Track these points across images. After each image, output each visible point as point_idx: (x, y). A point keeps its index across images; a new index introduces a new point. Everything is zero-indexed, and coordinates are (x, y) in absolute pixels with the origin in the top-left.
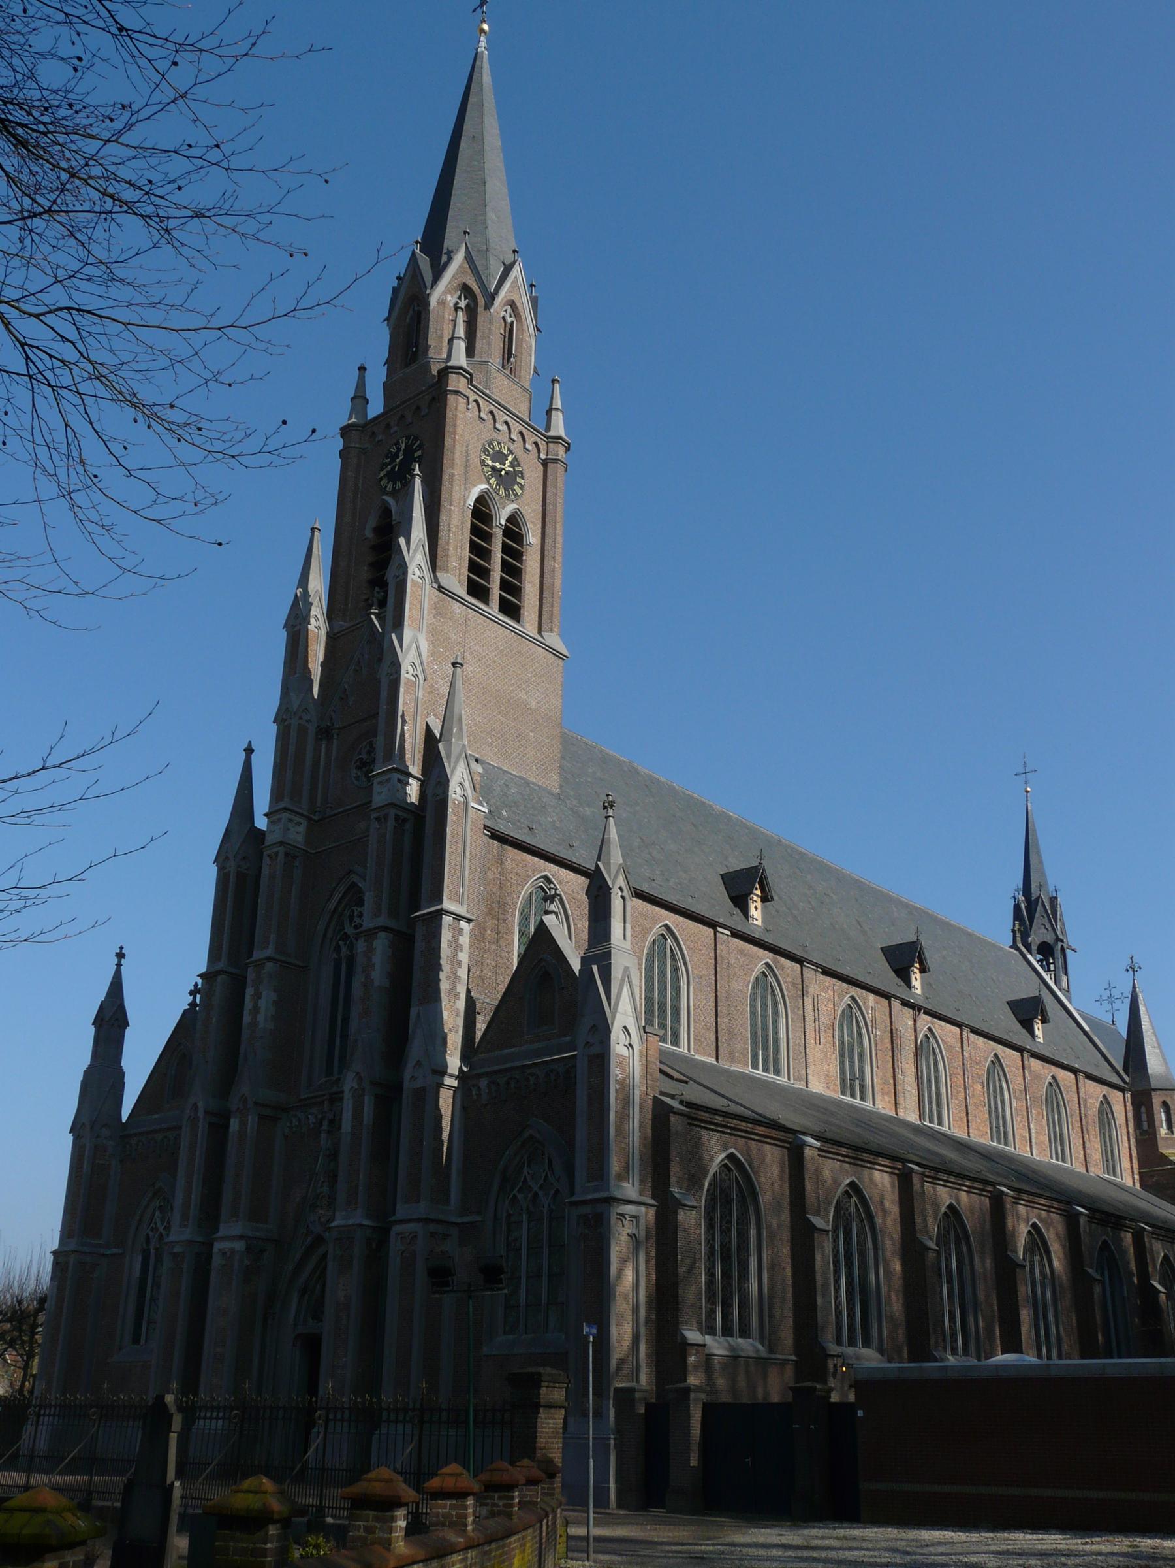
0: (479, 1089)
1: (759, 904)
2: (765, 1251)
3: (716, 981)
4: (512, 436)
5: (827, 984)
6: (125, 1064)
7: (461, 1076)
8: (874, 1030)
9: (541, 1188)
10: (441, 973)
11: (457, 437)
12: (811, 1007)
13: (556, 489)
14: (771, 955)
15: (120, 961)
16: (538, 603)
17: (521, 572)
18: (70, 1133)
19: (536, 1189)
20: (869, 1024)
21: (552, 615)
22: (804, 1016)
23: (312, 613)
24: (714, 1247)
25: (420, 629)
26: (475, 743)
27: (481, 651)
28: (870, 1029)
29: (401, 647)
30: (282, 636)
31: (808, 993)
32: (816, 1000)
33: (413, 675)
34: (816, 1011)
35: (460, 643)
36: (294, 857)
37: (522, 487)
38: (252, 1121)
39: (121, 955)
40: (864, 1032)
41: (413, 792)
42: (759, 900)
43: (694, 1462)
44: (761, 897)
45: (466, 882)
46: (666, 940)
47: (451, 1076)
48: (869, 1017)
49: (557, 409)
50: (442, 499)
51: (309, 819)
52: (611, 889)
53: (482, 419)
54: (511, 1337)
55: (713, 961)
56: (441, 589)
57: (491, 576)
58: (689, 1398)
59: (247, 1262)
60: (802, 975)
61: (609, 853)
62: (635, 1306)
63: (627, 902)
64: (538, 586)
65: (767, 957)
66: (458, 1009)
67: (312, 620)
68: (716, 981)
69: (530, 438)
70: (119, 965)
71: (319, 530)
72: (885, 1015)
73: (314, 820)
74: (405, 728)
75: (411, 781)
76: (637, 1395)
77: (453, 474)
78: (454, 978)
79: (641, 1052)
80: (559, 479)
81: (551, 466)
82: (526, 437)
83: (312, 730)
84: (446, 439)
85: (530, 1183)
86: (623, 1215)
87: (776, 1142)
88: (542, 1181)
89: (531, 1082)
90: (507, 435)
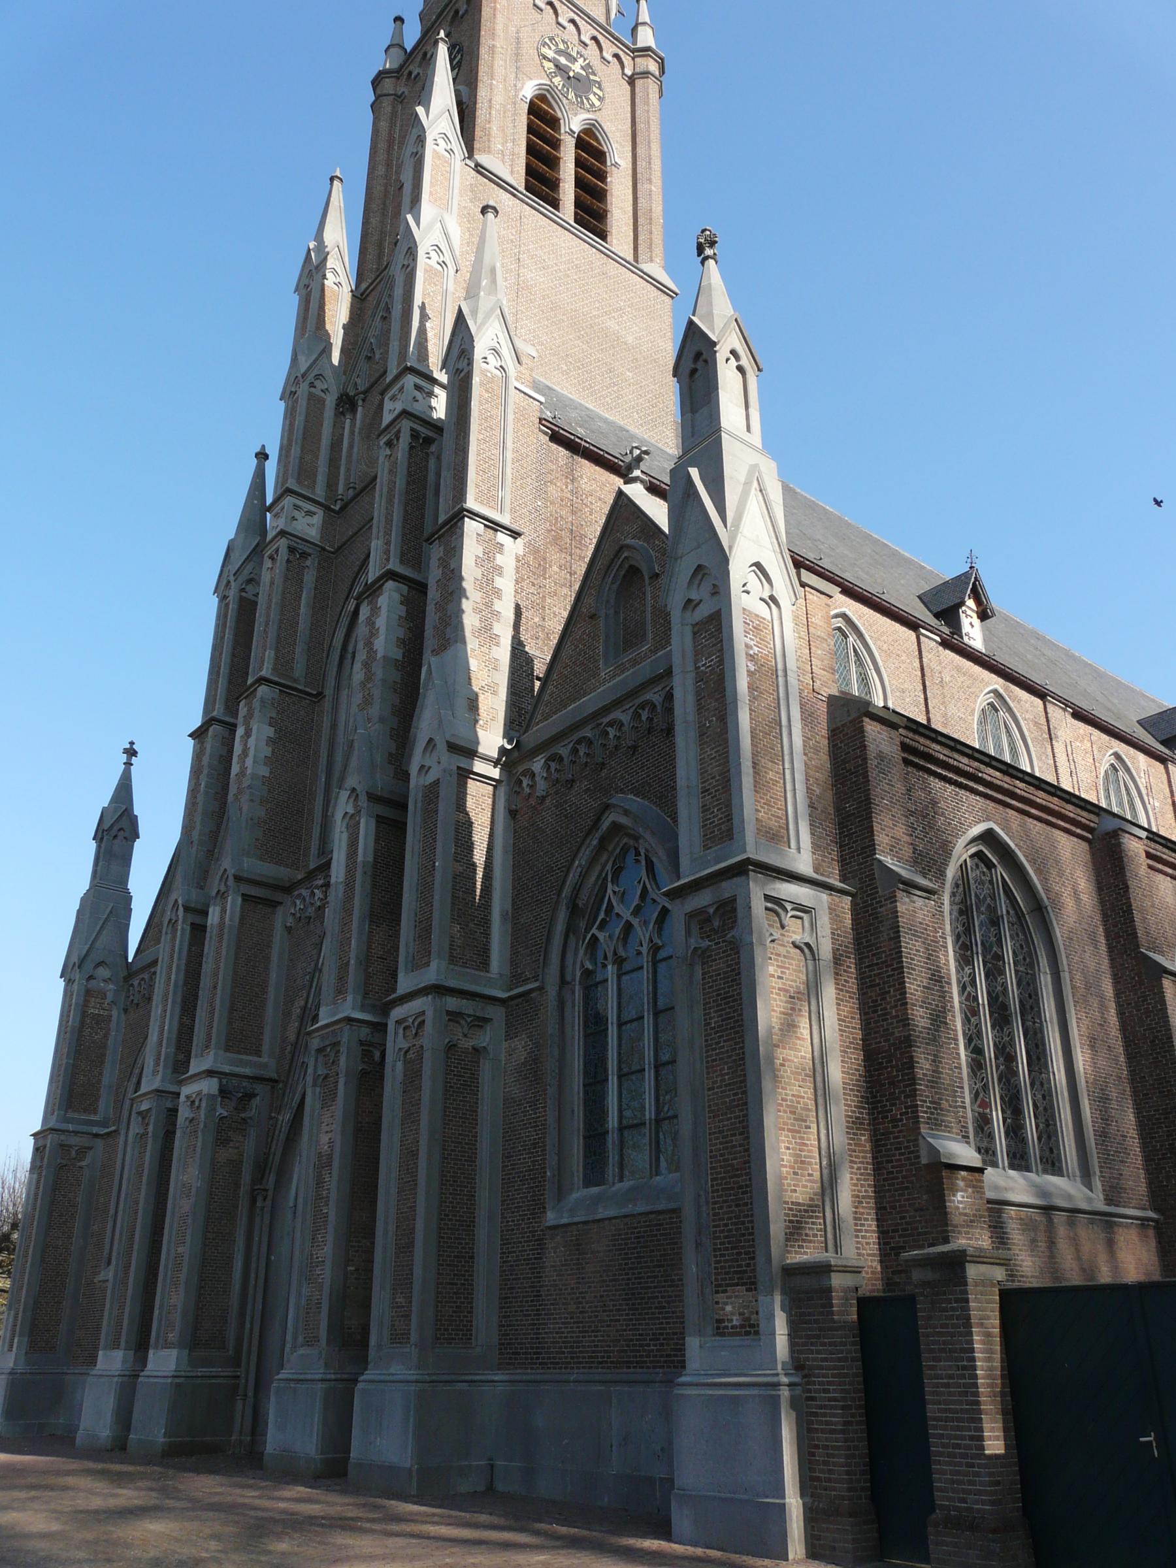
0: (533, 775)
1: (976, 621)
2: (1073, 1012)
3: (926, 699)
4: (583, 38)
5: (1081, 731)
6: (132, 886)
7: (506, 760)
8: (1151, 800)
9: (637, 911)
10: (464, 600)
11: (498, 6)
12: (1064, 755)
13: (648, 105)
14: (1001, 681)
15: (129, 759)
16: (632, 234)
17: (606, 196)
18: (61, 977)
19: (627, 914)
20: (1144, 792)
21: (651, 245)
22: (1056, 766)
23: (330, 264)
24: (976, 998)
25: (447, 207)
26: (541, 365)
27: (546, 257)
28: (1146, 798)
29: (418, 224)
30: (293, 302)
31: (1057, 737)
32: (1069, 747)
33: (439, 263)
34: (1072, 763)
35: (512, 241)
36: (304, 555)
37: (600, 99)
38: (234, 902)
39: (131, 752)
40: (1137, 801)
41: (439, 406)
42: (975, 615)
43: (994, 1444)
44: (977, 613)
45: (508, 482)
46: (846, 637)
47: (486, 759)
48: (1142, 783)
49: (644, 23)
50: (480, 74)
51: (327, 508)
52: (714, 344)
53: (538, 8)
54: (595, 1190)
55: (919, 673)
56: (479, 168)
57: (561, 189)
58: (965, 1277)
59: (220, 1111)
60: (1046, 713)
61: (710, 304)
62: (817, 1061)
63: (748, 376)
64: (631, 214)
65: (997, 683)
66: (497, 660)
67: (329, 275)
68: (926, 699)
69: (609, 50)
70: (128, 764)
71: (341, 180)
72: (1162, 783)
73: (333, 511)
74: (428, 325)
75: (437, 390)
76: (837, 1281)
77: (493, 46)
78: (489, 614)
79: (796, 618)
80: (651, 96)
81: (639, 83)
82: (603, 44)
83: (330, 401)
84: (483, 9)
85: (618, 908)
86: (777, 901)
87: (1072, 827)
88: (636, 901)
89: (611, 736)
90: (577, 37)
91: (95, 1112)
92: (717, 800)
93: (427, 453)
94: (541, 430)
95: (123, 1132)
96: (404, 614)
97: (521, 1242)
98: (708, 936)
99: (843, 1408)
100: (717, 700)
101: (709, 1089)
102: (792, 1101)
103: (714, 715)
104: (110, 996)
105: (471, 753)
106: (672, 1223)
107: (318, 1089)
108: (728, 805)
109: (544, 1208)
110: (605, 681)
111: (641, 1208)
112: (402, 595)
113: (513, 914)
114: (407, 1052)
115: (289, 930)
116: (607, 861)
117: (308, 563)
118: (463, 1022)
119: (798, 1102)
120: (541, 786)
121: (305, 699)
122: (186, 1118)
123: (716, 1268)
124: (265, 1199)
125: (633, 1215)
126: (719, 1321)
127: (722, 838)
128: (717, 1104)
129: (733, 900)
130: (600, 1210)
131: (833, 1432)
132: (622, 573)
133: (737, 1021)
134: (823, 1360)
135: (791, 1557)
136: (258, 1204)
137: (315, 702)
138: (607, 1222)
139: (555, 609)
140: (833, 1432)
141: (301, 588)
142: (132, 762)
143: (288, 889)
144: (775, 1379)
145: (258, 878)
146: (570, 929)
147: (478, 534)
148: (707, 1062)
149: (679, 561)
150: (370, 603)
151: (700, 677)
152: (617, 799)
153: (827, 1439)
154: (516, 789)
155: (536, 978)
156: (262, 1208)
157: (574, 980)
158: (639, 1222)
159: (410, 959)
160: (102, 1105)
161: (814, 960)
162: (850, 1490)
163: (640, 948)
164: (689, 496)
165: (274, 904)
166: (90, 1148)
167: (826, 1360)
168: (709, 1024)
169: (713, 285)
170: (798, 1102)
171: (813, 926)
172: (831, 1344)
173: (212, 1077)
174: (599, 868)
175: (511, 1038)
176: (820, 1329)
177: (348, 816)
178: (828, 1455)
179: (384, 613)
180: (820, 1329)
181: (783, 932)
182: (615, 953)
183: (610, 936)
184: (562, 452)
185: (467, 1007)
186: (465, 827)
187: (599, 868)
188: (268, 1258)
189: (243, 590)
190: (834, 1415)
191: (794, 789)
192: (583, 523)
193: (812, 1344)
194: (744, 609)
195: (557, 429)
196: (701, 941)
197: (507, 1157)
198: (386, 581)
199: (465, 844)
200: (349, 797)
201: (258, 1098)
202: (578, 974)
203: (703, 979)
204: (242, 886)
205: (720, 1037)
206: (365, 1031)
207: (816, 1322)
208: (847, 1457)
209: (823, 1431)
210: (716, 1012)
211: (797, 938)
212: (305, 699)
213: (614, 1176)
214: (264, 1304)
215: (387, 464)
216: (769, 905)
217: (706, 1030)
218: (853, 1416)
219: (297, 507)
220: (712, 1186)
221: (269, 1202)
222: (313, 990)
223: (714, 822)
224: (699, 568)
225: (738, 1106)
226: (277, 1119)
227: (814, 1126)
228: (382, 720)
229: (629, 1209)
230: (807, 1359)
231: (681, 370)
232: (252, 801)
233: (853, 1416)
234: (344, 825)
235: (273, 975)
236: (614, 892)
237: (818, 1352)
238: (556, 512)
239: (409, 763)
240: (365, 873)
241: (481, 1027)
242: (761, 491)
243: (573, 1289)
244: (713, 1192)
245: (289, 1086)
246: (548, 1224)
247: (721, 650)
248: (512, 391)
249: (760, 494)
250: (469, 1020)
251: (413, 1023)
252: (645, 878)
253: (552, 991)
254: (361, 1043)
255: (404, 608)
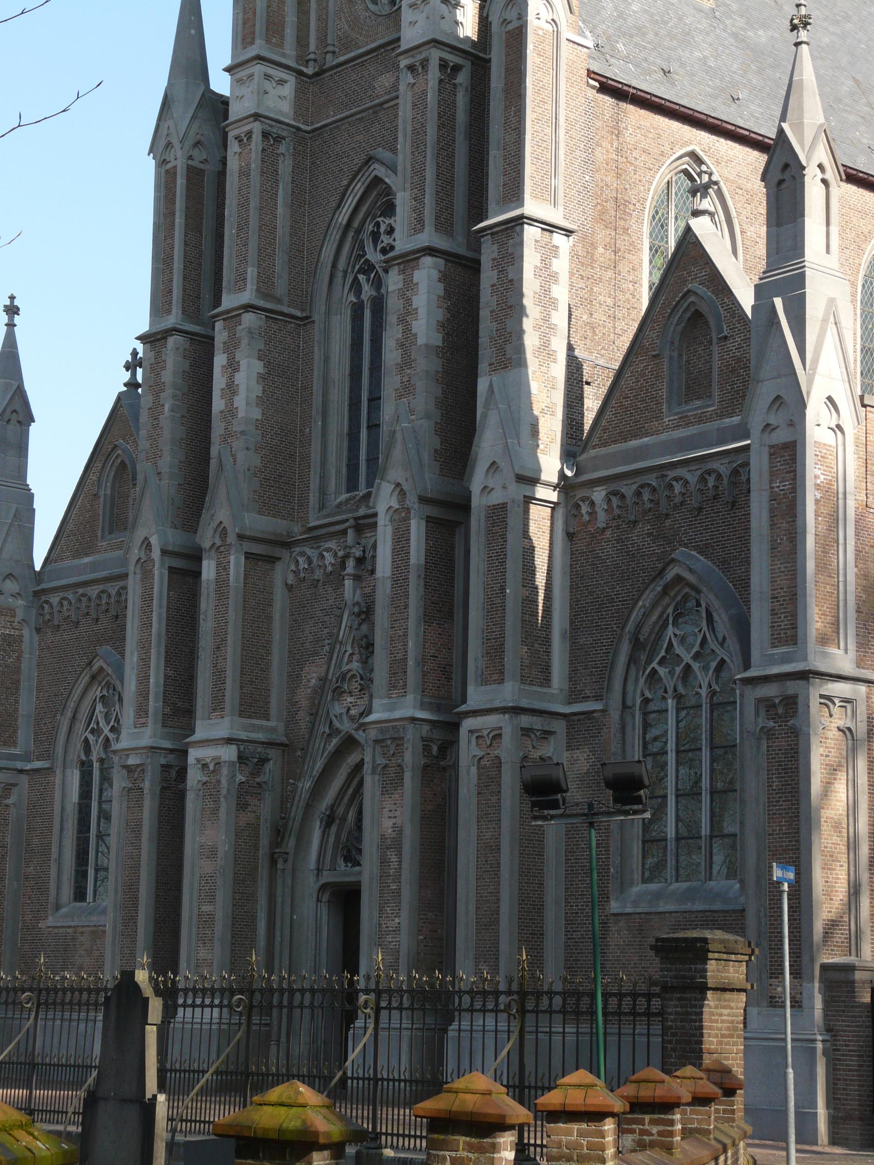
0: (592, 504)
6: (32, 480)
7: (564, 485)
9: (697, 657)
15: (11, 319)
19: (687, 658)
36: (279, 139)
38: (236, 562)
39: (12, 310)
47: (547, 484)
52: (804, 168)
54: (653, 887)
59: (240, 778)
63: (831, 189)
70: (11, 325)
76: (858, 975)
78: (546, 327)
86: (829, 698)
88: (696, 648)
89: (676, 491)
91: (14, 744)
92: (785, 608)
93: (455, 85)
94: (588, 85)
95: (58, 771)
96: (442, 293)
97: (585, 924)
98: (773, 719)
99: (858, 1056)
100: (788, 522)
101: (770, 835)
102: (831, 848)
103: (785, 535)
104: (20, 614)
105: (534, 480)
106: (726, 920)
107: (377, 777)
108: (794, 615)
109: (608, 898)
110: (667, 428)
111: (698, 906)
112: (440, 271)
113: (571, 633)
114: (481, 758)
115: (290, 588)
116: (668, 605)
117: (282, 149)
118: (533, 736)
119: (836, 848)
120: (602, 518)
121: (291, 323)
122: (199, 781)
123: (771, 961)
124: (286, 861)
125: (692, 912)
126: (771, 997)
127: (787, 641)
128: (776, 847)
129: (795, 697)
130: (662, 904)
131: (850, 1070)
132: (688, 315)
133: (794, 788)
134: (846, 1026)
135: (819, 1143)
136: (280, 866)
137: (300, 325)
138: (667, 915)
139: (601, 297)
140: (850, 1070)
141: (277, 182)
142: (16, 322)
143: (287, 544)
144: (813, 1037)
145: (260, 536)
146: (632, 660)
147: (536, 241)
148: (769, 814)
149: (760, 384)
150: (402, 272)
151: (773, 498)
152: (680, 553)
153: (846, 1075)
154: (574, 512)
155: (598, 698)
156: (283, 870)
157: (634, 705)
158: (697, 917)
159: (479, 673)
160: (21, 735)
161: (853, 740)
162: (859, 1105)
163: (699, 690)
164: (772, 325)
165: (272, 560)
166: (15, 785)
167: (849, 1026)
168: (771, 786)
169: (805, 82)
170: (836, 848)
171: (854, 713)
172: (852, 1016)
173: (231, 744)
174: (659, 609)
175: (572, 750)
176: (845, 1007)
177: (391, 511)
178: (847, 1085)
179: (423, 289)
180: (845, 1007)
181: (831, 719)
182: (675, 690)
183: (669, 672)
184: (608, 101)
185: (536, 722)
186: (530, 550)
187: (659, 609)
188: (292, 918)
189: (190, 158)
190: (853, 1061)
191: (846, 600)
192: (628, 186)
193: (839, 1016)
194: (815, 442)
195: (604, 80)
196: (766, 721)
197: (570, 852)
198: (424, 255)
199: (530, 570)
200: (393, 491)
201: (271, 762)
202: (639, 701)
203: (768, 751)
204: (244, 544)
205: (780, 797)
206: (426, 728)
207: (843, 1001)
208: (859, 1086)
209: (844, 1070)
210: (777, 778)
211: (841, 723)
212: (291, 323)
213: (672, 877)
214: (290, 958)
215: (410, 94)
216: (822, 701)
217: (768, 790)
218: (864, 1061)
219: (268, 77)
220: (770, 904)
221: (290, 865)
222: (334, 662)
223: (780, 626)
224: (778, 397)
225: (792, 850)
226: (297, 787)
227: (846, 865)
228: (427, 416)
229: (688, 906)
230: (836, 1025)
231: (768, 176)
232: (248, 449)
233: (864, 1061)
234: (388, 518)
235: (277, 636)
236: (675, 635)
237: (843, 1021)
238: (602, 180)
239: (470, 480)
240: (419, 576)
241: (546, 738)
242: (836, 324)
243: (636, 964)
244: (770, 908)
245: (309, 755)
246: (612, 911)
247: (794, 479)
248: (564, 44)
249: (834, 326)
250: (538, 734)
251: (488, 735)
252: (705, 628)
253: (615, 715)
254: (423, 739)
255: (441, 286)
